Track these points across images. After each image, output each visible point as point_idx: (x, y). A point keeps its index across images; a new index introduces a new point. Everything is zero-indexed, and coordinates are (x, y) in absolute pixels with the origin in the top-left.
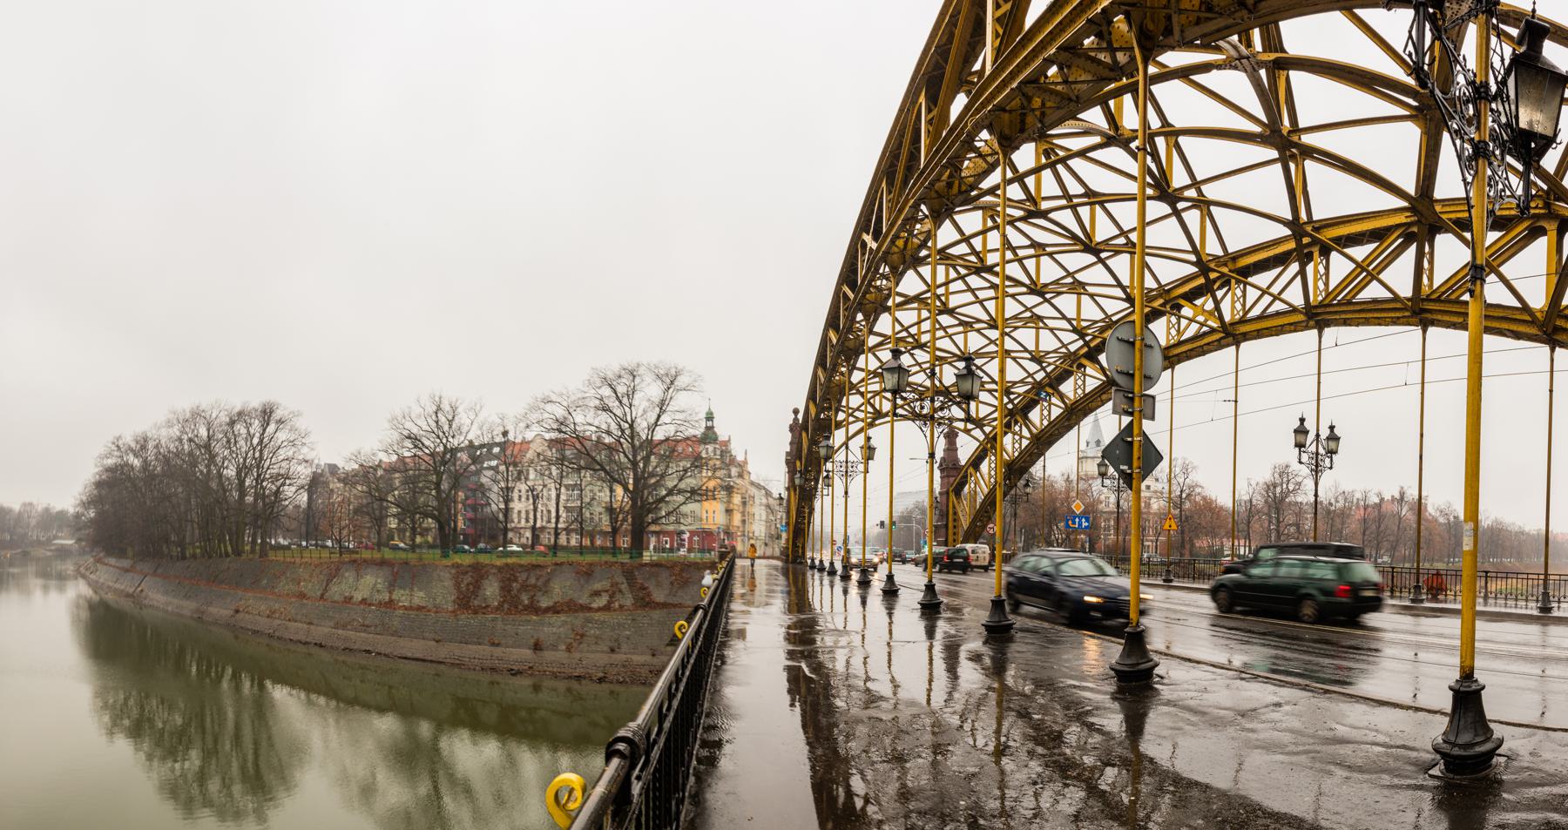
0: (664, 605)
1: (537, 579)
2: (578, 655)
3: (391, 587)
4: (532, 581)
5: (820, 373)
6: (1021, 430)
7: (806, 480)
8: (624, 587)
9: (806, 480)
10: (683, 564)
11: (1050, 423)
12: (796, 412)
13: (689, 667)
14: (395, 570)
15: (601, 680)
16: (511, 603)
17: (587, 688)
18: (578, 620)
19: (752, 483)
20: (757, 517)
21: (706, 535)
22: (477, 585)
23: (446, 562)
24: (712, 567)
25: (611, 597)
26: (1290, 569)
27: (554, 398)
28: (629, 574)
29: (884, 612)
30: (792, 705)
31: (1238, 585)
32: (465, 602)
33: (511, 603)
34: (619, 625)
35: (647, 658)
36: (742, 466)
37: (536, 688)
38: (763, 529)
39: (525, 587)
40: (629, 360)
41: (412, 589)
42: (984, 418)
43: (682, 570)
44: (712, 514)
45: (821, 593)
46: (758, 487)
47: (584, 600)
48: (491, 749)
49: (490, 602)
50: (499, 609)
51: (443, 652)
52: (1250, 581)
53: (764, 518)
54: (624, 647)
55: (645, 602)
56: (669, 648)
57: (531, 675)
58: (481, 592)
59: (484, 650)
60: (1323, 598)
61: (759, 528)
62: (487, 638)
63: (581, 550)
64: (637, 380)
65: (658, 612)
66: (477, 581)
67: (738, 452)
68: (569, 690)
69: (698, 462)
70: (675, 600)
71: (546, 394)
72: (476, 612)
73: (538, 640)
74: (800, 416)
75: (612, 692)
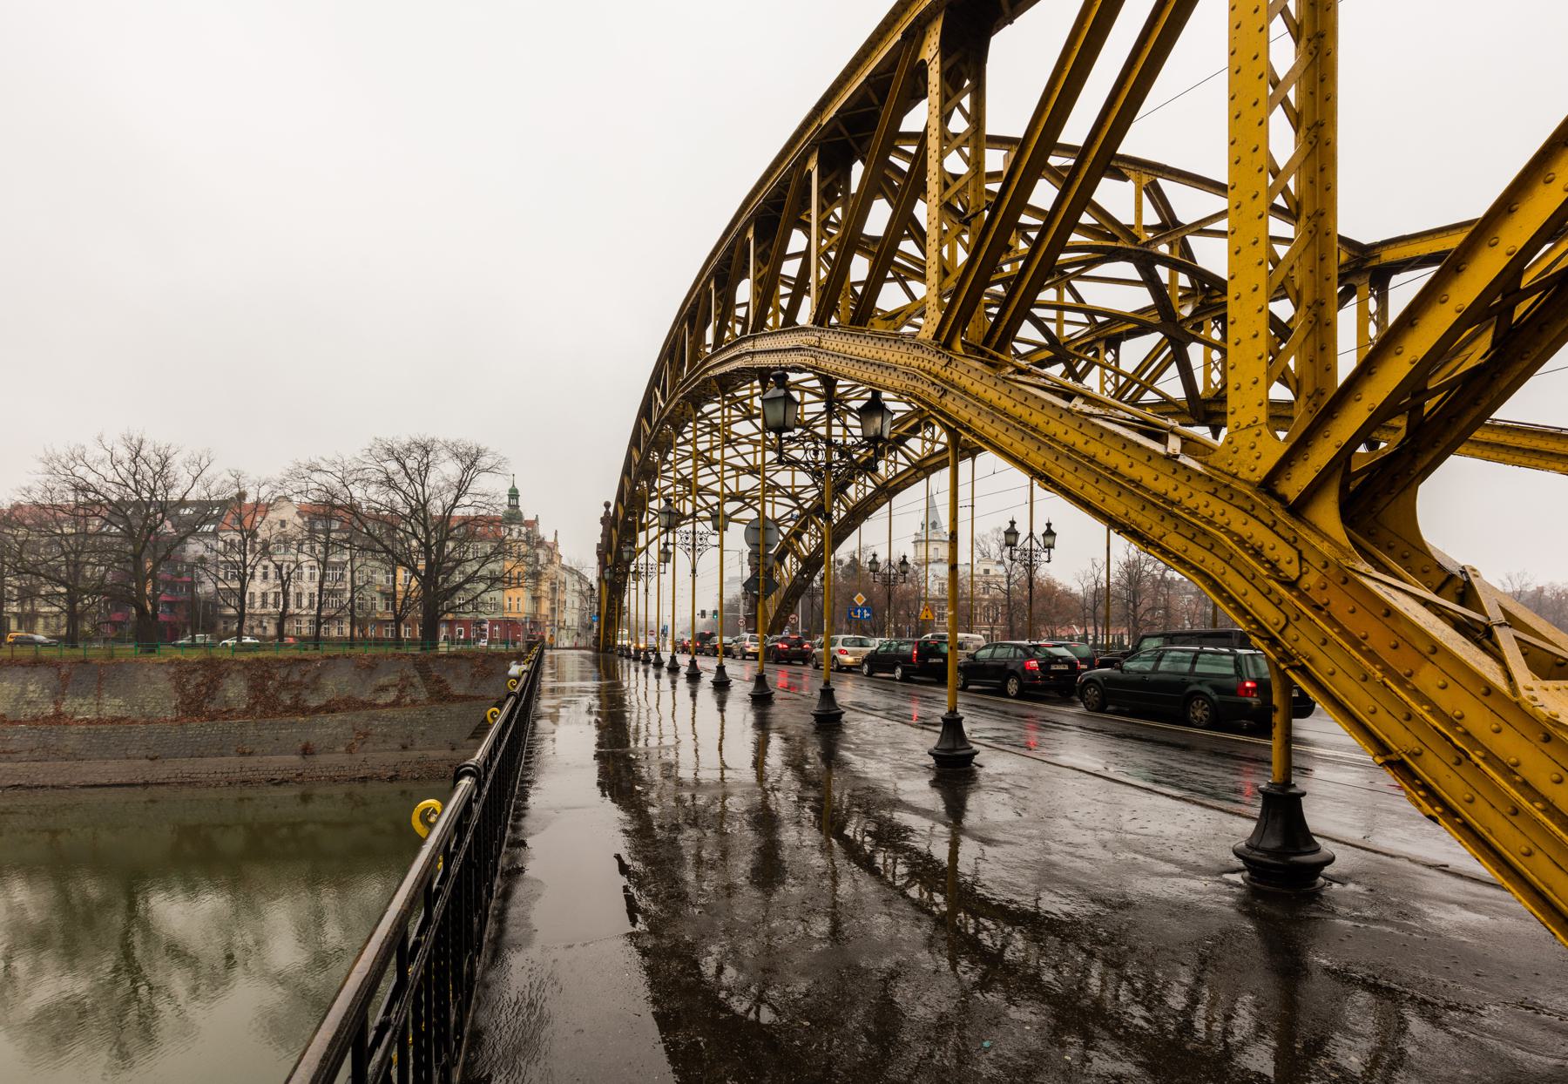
0: (464, 698)
1: (303, 676)
2: (362, 756)
3: (57, 696)
4: (296, 677)
5: (635, 453)
6: (923, 447)
7: (616, 574)
8: (417, 680)
9: (616, 574)
10: (484, 655)
11: (839, 521)
12: (607, 505)
13: (493, 770)
14: (63, 671)
15: (392, 779)
16: (264, 703)
17: (374, 788)
18: (361, 718)
19: (564, 568)
20: (569, 605)
21: (510, 625)
22: (213, 686)
23: (154, 658)
24: (519, 658)
25: (401, 691)
26: (1175, 661)
27: (324, 466)
28: (422, 667)
29: (715, 706)
30: (604, 795)
31: (1109, 681)
32: (193, 707)
33: (264, 703)
34: (412, 720)
35: (447, 753)
36: (552, 548)
37: (306, 798)
38: (576, 618)
39: (285, 685)
40: (423, 433)
41: (99, 696)
42: (779, 519)
43: (484, 662)
44: (517, 602)
45: (638, 685)
46: (571, 571)
47: (366, 696)
48: (211, 903)
49: (234, 704)
50: (250, 710)
51: (162, 771)
52: (1125, 676)
53: (577, 605)
54: (419, 743)
55: (442, 696)
56: (471, 741)
57: (302, 782)
58: (219, 694)
59: (230, 763)
60: (1215, 697)
61: (571, 617)
62: (234, 748)
63: (351, 642)
64: (431, 457)
65: (458, 705)
66: (212, 681)
67: (545, 532)
68: (349, 795)
69: (501, 550)
70: (477, 693)
71: (313, 460)
72: (212, 718)
73: (308, 744)
74: (611, 510)
75: (403, 793)
